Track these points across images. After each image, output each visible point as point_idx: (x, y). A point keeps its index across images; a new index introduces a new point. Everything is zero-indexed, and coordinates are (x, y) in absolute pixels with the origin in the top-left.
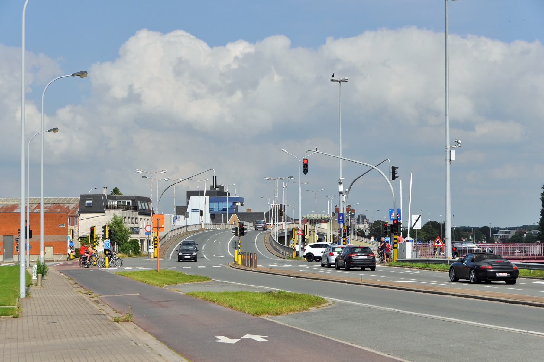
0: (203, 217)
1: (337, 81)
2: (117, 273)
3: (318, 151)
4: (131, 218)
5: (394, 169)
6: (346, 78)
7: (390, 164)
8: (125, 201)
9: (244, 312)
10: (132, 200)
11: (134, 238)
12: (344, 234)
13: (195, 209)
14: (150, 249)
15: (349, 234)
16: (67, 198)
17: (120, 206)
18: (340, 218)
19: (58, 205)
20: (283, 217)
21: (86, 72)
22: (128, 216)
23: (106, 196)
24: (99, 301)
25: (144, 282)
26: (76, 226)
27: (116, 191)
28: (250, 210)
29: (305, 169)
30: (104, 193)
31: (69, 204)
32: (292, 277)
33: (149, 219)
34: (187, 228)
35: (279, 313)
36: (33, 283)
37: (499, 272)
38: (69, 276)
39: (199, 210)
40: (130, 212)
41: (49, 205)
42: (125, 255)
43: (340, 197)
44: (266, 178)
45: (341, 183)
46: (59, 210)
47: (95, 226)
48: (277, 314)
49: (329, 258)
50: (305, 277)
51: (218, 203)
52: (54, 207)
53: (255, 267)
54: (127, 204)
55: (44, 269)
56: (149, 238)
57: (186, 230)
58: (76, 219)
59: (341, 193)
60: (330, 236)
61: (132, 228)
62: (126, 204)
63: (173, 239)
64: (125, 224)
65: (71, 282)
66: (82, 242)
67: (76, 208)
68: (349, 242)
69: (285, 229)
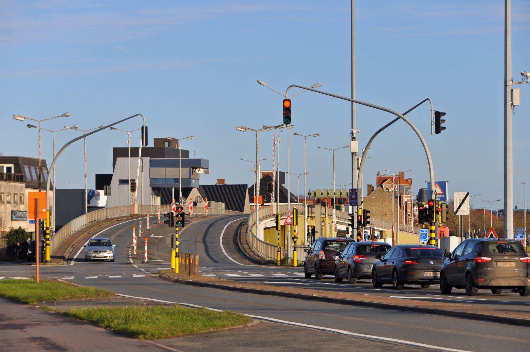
0: (136, 194)
5: (438, 115)
8: (3, 167)
18: (353, 197)
20: (274, 193)
28: (223, 181)
51: (165, 168)
57: (105, 215)
61: (14, 211)
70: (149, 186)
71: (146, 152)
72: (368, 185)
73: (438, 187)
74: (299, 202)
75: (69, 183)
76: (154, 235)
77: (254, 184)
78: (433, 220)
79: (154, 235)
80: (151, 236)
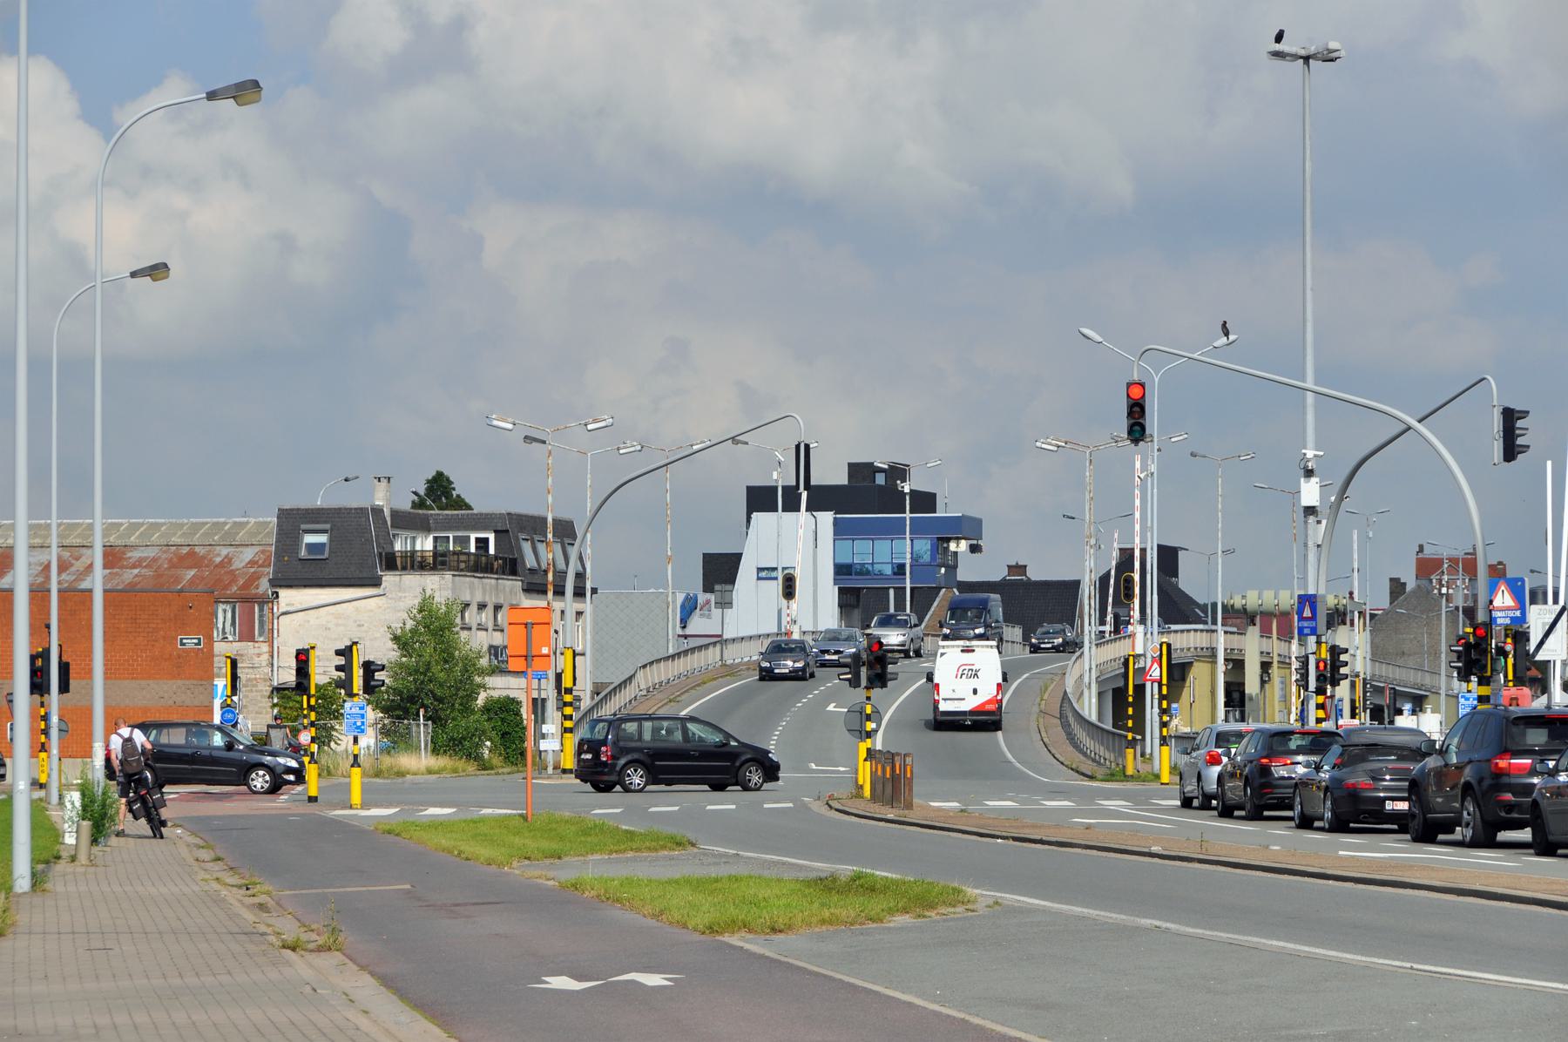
0: (794, 604)
1: (1296, 57)
2: (380, 827)
3: (1232, 337)
4: (490, 609)
6: (1333, 45)
7: (1496, 396)
8: (469, 537)
9: (685, 926)
10: (495, 532)
11: (504, 693)
12: (1318, 679)
13: (767, 569)
14: (543, 736)
15: (1337, 676)
16: (226, 523)
17: (444, 555)
19: (185, 550)
20: (1137, 601)
21: (255, 84)
22: (479, 598)
23: (387, 513)
24: (269, 905)
25: (456, 853)
26: (261, 639)
27: (439, 488)
28: (1019, 569)
29: (1133, 421)
30: (378, 503)
31: (231, 549)
32: (999, 841)
33: (582, 613)
34: (725, 651)
35: (783, 927)
36: (64, 854)
37: (1393, 799)
38: (201, 836)
39: (780, 570)
40: (489, 581)
41: (150, 553)
42: (461, 764)
43: (1306, 528)
44: (1038, 444)
45: (1309, 473)
46: (192, 572)
47: (313, 648)
48: (774, 930)
49: (1203, 773)
50: (1039, 837)
52: (170, 561)
53: (909, 806)
54: (477, 548)
55: (104, 805)
56: (539, 689)
57: (718, 658)
58: (261, 610)
59: (1310, 511)
60: (961, 697)
62: (473, 549)
63: (660, 696)
64: (464, 635)
65: (205, 855)
66: (285, 708)
67: (259, 567)
68: (1341, 710)
69: (1144, 655)
70: (832, 583)
71: (822, 498)
72: (1392, 580)
73: (1505, 592)
74: (1210, 623)
75: (636, 576)
76: (835, 707)
77: (1109, 572)
78: (1486, 672)
79: (835, 707)
80: (828, 709)
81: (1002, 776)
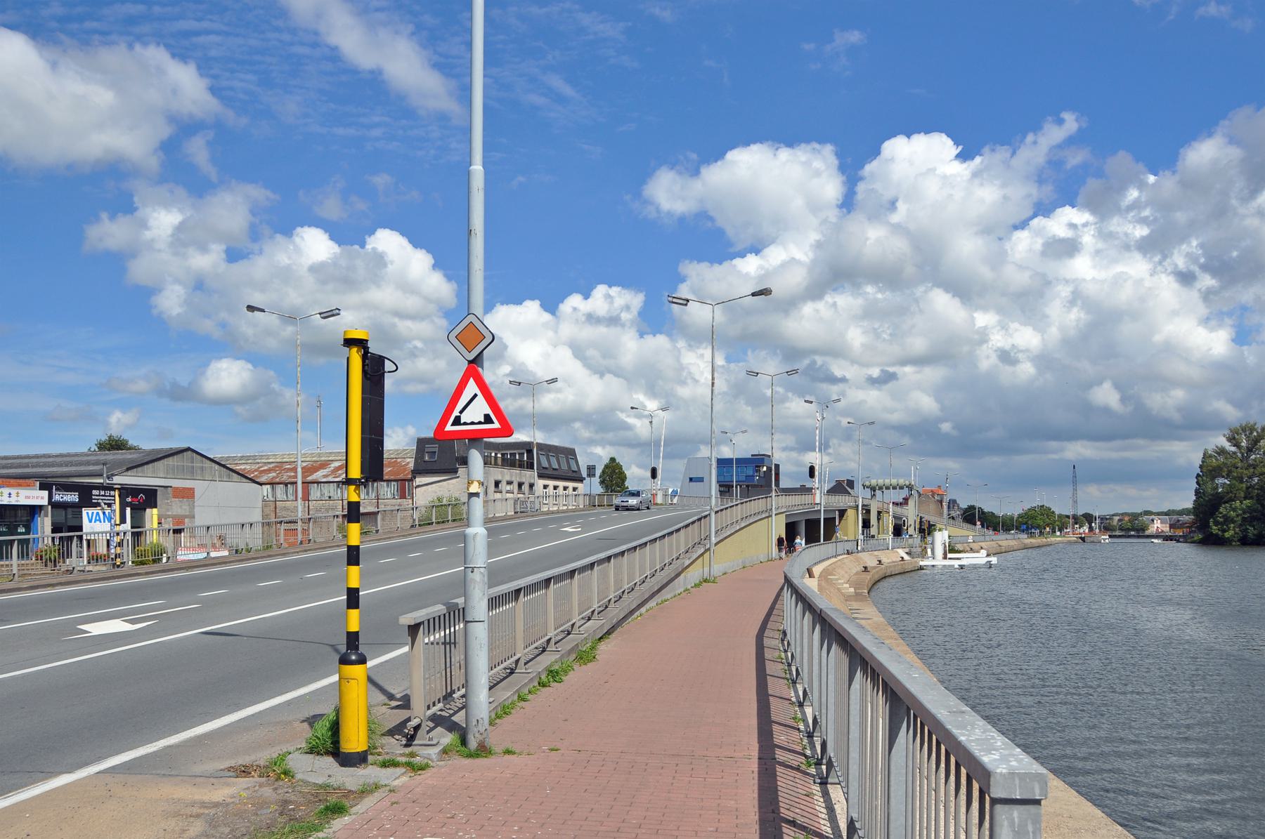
22: (508, 478)
81: (559, 391)
